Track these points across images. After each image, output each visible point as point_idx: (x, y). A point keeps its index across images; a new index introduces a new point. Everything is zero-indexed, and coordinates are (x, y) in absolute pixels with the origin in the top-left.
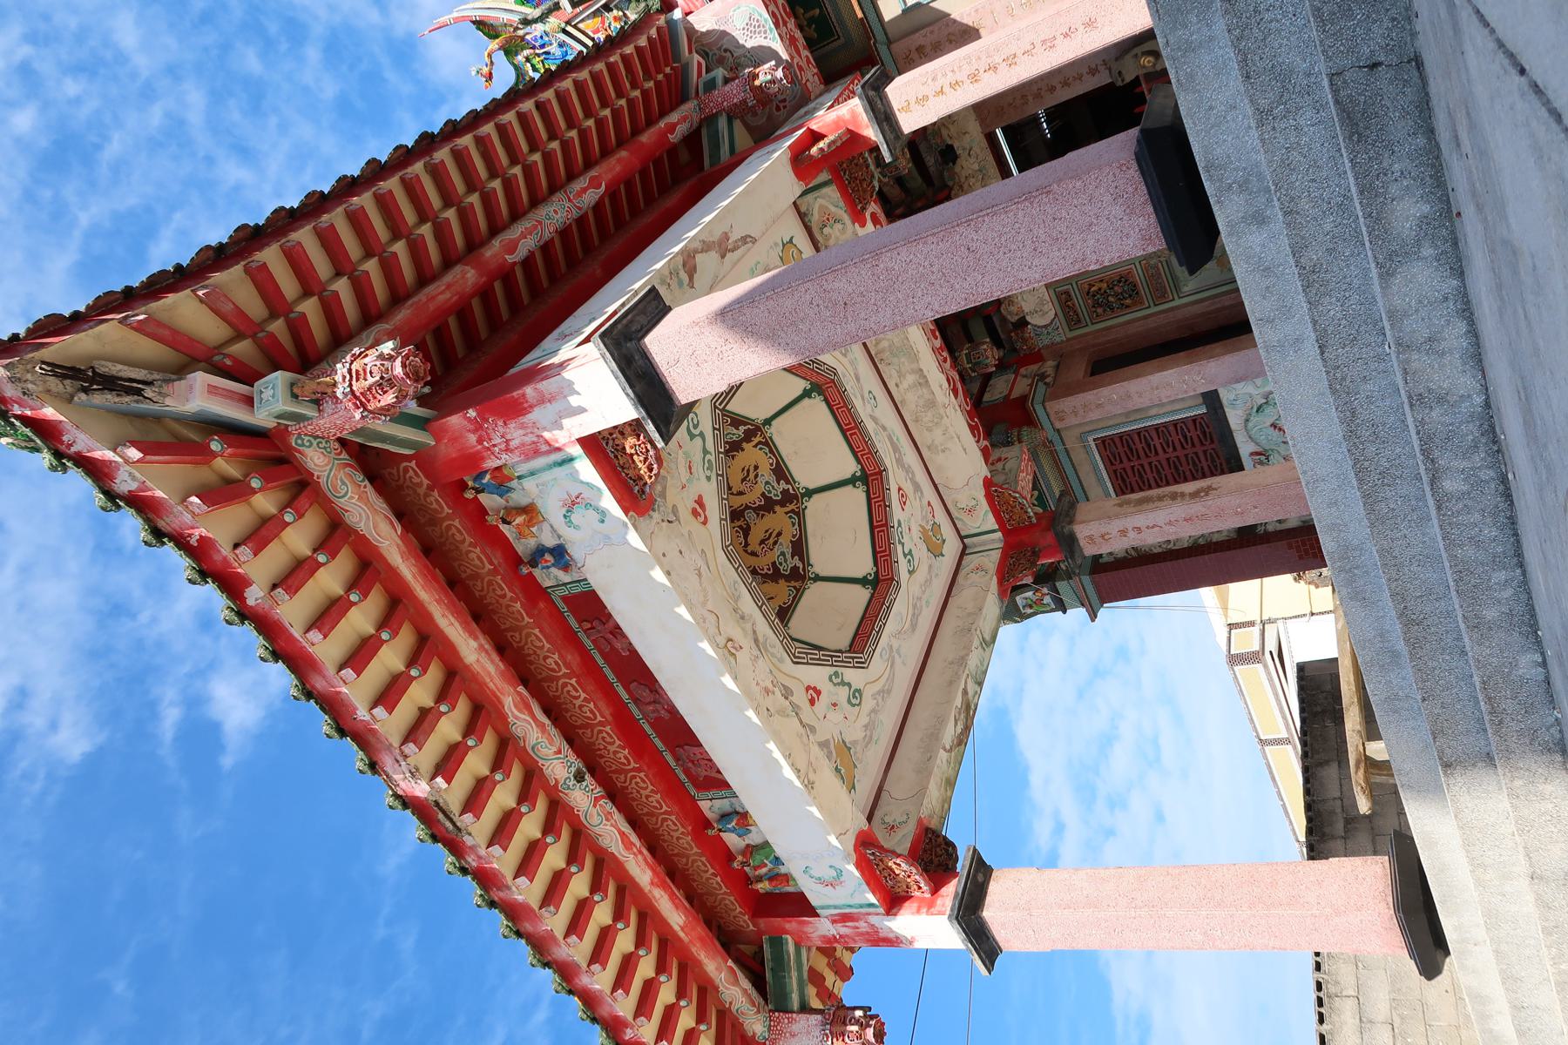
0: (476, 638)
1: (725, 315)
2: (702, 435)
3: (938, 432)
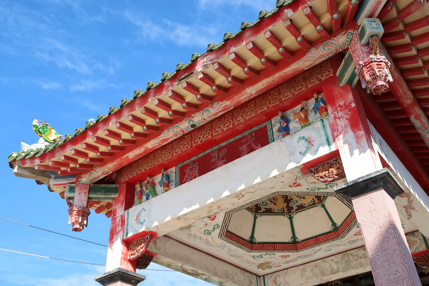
0: (256, 93)
1: (393, 226)
2: (327, 188)
3: (310, 274)
